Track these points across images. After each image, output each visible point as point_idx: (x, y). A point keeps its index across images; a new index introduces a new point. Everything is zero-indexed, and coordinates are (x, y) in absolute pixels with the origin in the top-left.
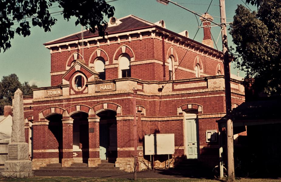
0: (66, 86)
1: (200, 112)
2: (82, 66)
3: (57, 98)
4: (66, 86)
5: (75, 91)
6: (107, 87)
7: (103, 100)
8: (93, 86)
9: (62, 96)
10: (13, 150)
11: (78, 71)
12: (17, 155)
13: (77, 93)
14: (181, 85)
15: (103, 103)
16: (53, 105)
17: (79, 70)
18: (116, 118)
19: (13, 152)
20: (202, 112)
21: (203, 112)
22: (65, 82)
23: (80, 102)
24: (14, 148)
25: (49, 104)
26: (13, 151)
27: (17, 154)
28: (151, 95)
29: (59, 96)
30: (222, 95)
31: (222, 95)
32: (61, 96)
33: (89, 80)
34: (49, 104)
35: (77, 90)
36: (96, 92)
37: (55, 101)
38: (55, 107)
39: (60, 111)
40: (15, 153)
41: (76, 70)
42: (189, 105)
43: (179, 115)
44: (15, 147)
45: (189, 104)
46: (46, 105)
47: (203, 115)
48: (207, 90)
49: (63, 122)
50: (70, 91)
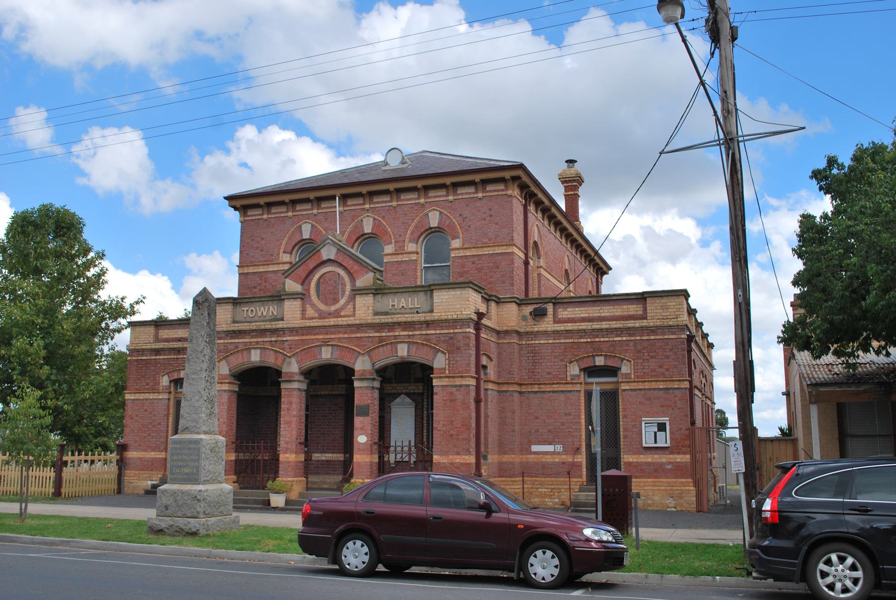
0: (293, 296)
1: (439, 369)
2: (341, 250)
3: (268, 326)
4: (293, 296)
5: (317, 310)
6: (407, 304)
7: (397, 334)
8: (369, 299)
9: (282, 319)
10: (185, 455)
11: (329, 260)
12: (198, 471)
13: (322, 316)
14: (577, 309)
15: (397, 341)
16: (257, 343)
17: (332, 258)
18: (432, 379)
19: (184, 460)
20: (445, 369)
21: (447, 372)
22: (292, 286)
23: (332, 336)
24: (189, 449)
25: (244, 340)
26: (184, 457)
27: (198, 468)
28: (505, 328)
29: (271, 320)
30: (468, 330)
31: (468, 330)
32: (278, 320)
33: (359, 283)
34: (244, 340)
35: (322, 307)
36: (376, 314)
37: (263, 332)
38: (261, 348)
39: (276, 358)
40: (189, 464)
41: (325, 258)
42: (597, 359)
43: (572, 379)
44: (193, 446)
45: (597, 355)
46: (237, 341)
47: (634, 382)
48: (644, 323)
49: (283, 386)
50: (304, 311)
